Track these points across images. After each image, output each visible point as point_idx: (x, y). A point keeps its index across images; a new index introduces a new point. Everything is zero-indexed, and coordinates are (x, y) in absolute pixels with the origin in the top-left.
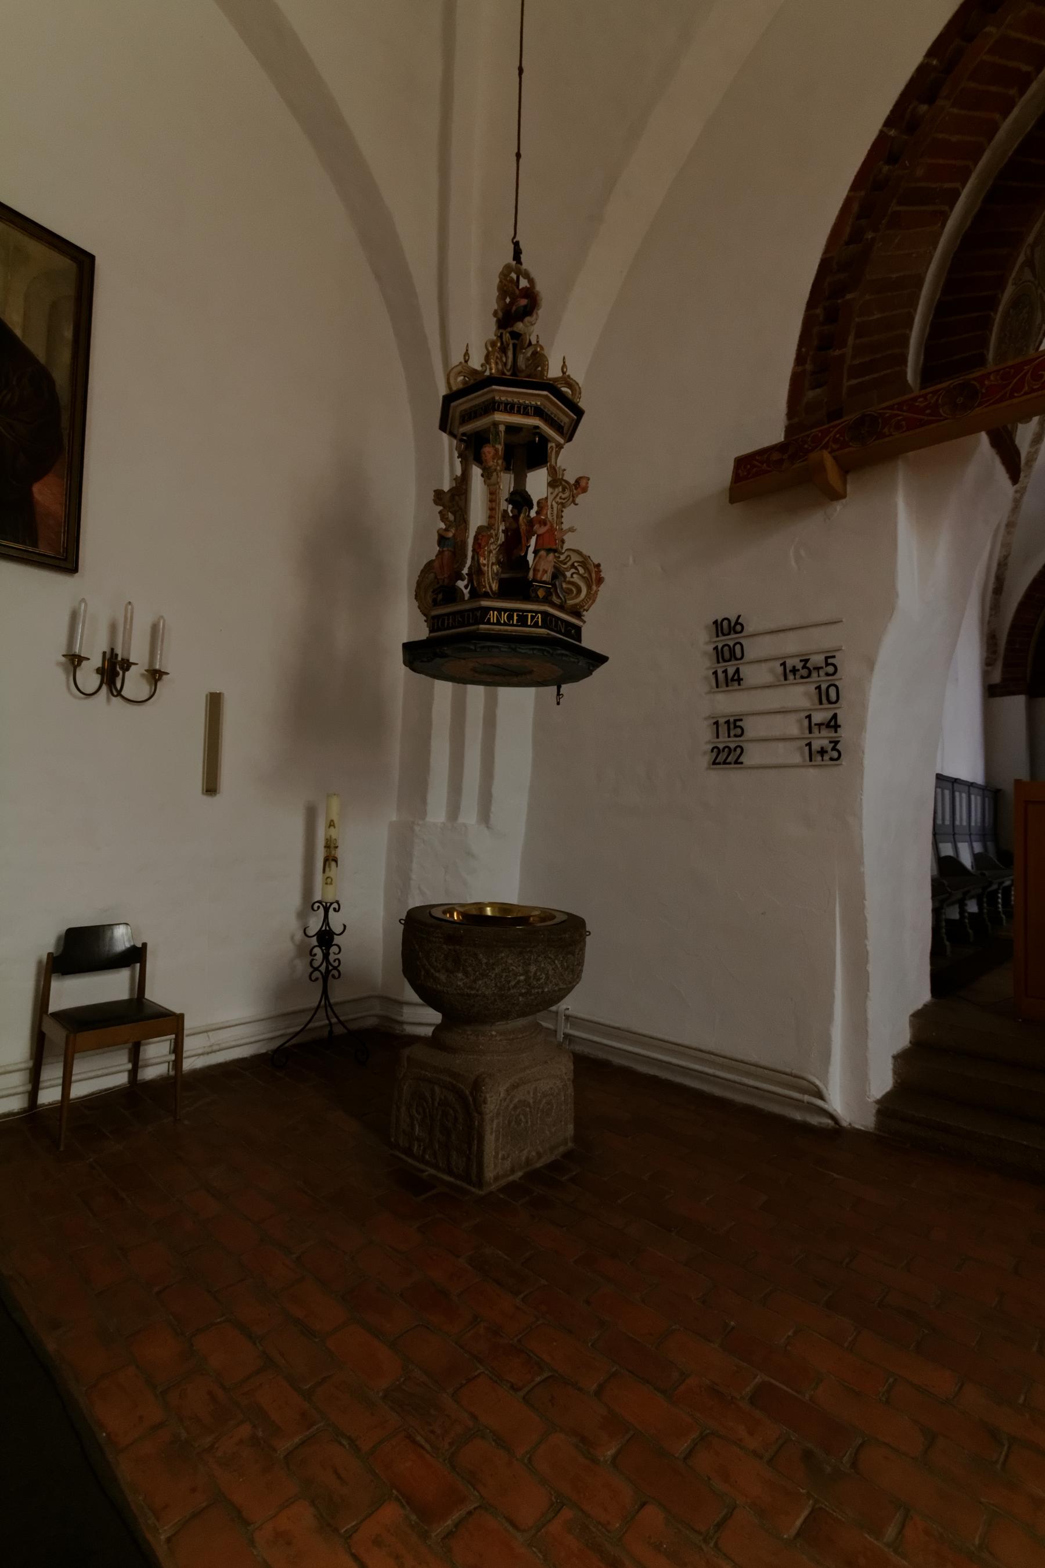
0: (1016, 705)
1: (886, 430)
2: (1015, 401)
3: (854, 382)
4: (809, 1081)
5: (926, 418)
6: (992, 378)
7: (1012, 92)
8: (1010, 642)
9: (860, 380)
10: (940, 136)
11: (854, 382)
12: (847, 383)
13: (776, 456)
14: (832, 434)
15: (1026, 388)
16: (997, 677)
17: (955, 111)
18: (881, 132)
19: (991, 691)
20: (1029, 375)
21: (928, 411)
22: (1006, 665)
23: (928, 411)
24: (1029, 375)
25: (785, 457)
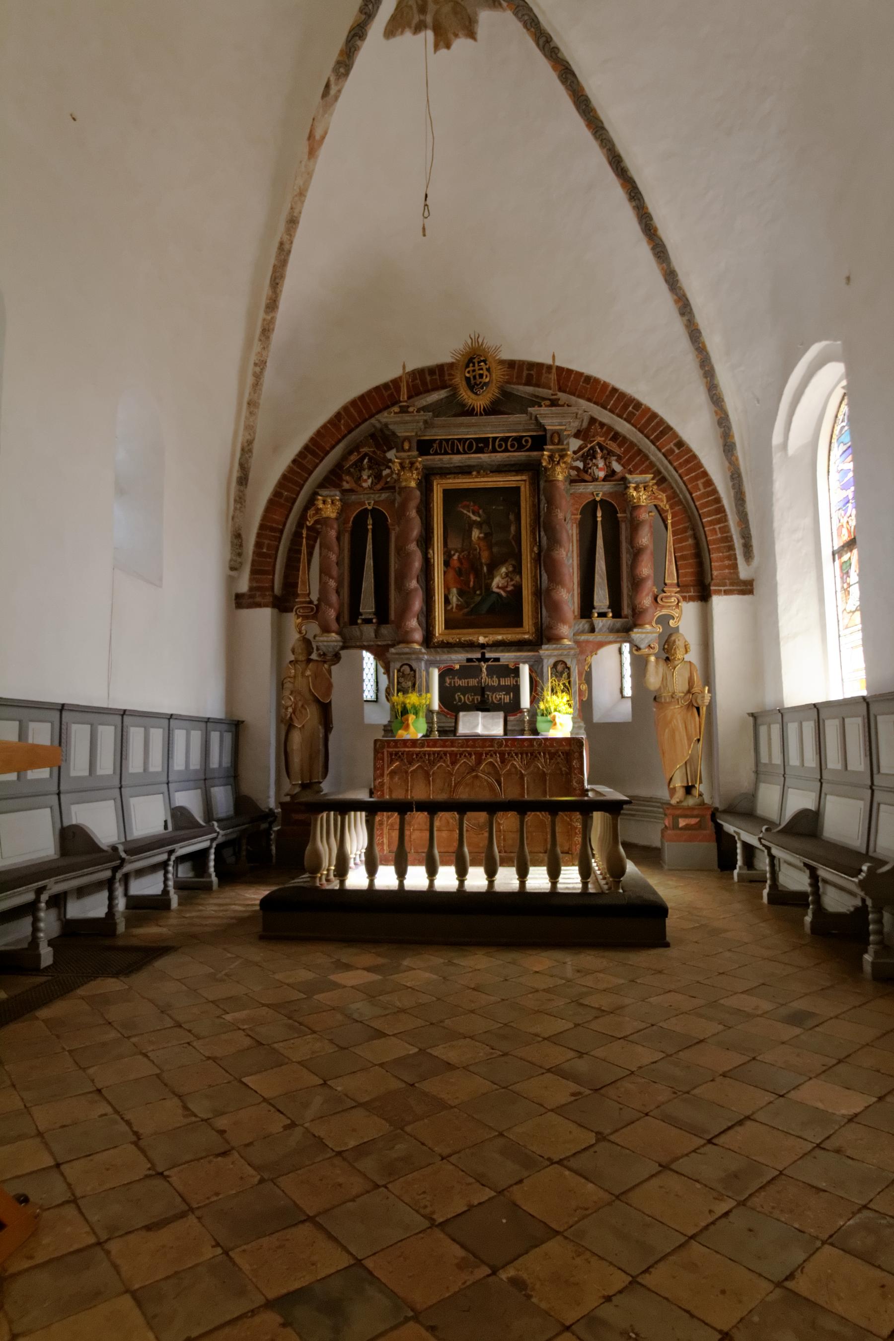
0: (262, 618)
8: (258, 545)
16: (244, 586)
19: (240, 601)
22: (254, 572)
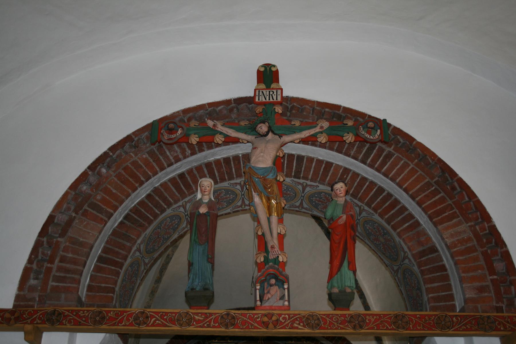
1: (64, 321)
2: (119, 327)
3: (55, 284)
4: (140, 285)
5: (82, 322)
6: (111, 313)
7: (137, 185)
9: (57, 284)
10: (109, 187)
11: (55, 284)
12: (52, 283)
13: (7, 315)
14: (38, 314)
15: (123, 323)
17: (116, 179)
18: (86, 170)
20: (125, 318)
21: (84, 319)
23: (84, 319)
24: (125, 318)
25: (13, 317)
